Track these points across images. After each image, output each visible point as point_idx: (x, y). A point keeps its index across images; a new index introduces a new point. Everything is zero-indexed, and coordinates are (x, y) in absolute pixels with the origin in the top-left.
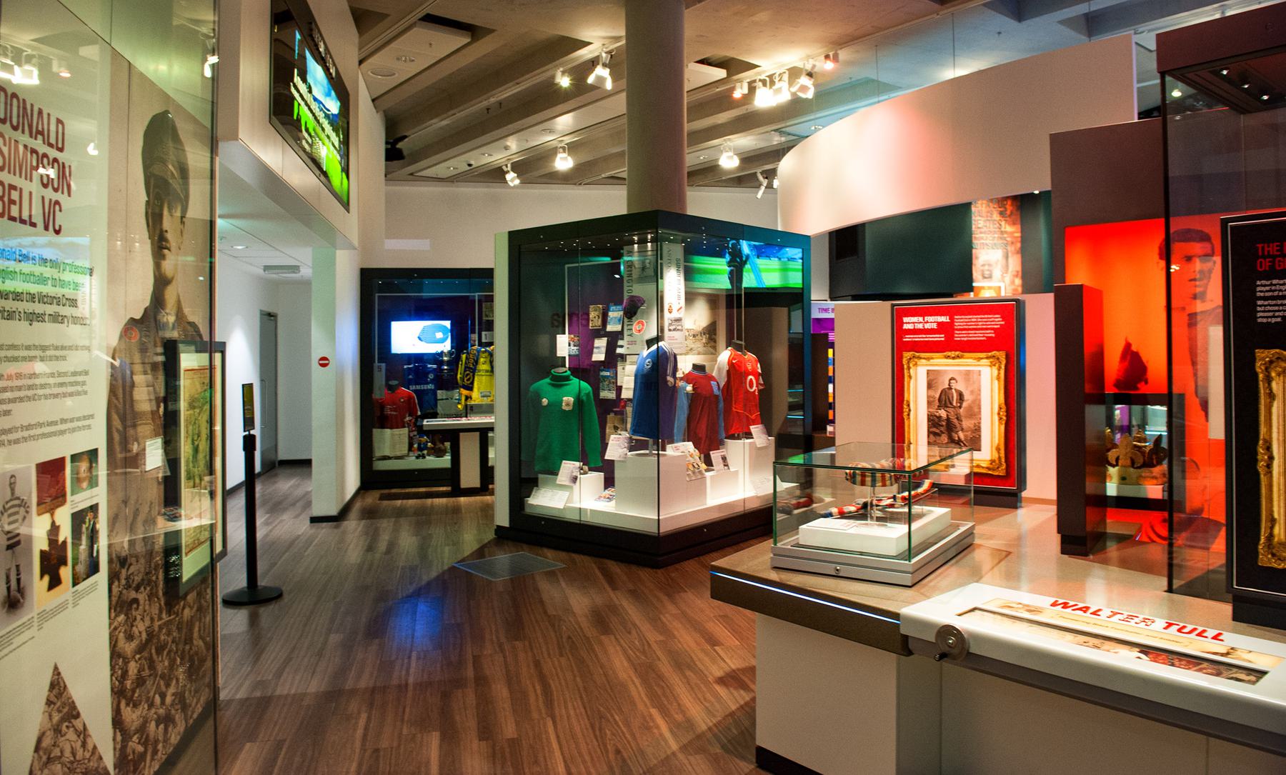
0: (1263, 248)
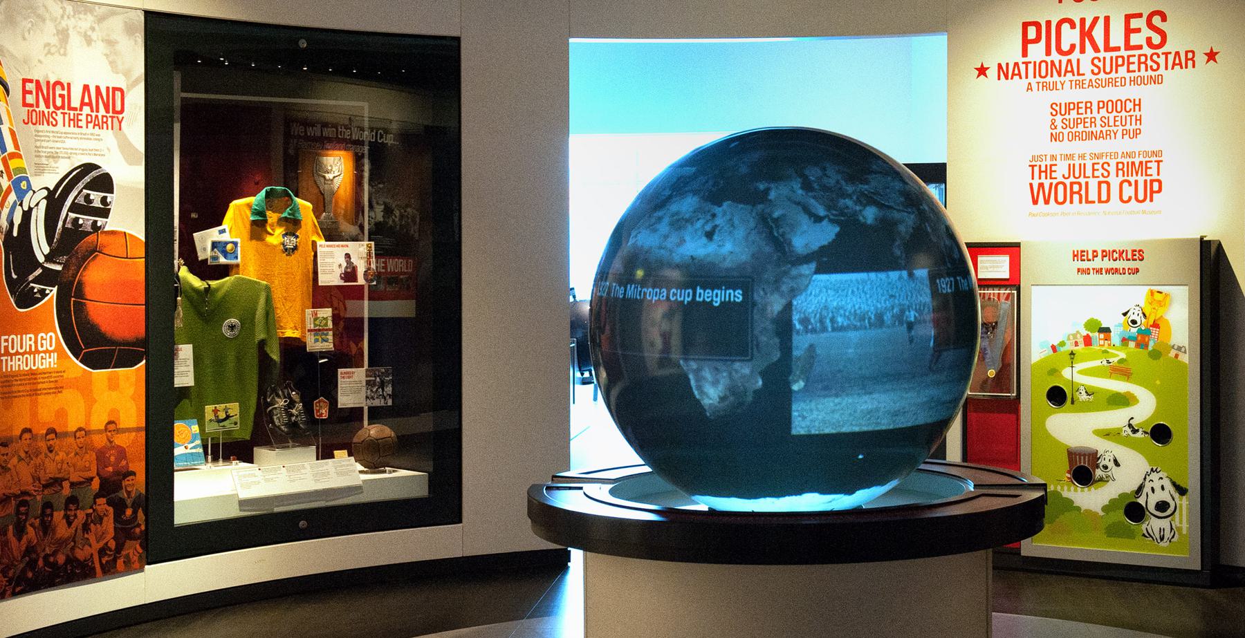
0: (7, 360)
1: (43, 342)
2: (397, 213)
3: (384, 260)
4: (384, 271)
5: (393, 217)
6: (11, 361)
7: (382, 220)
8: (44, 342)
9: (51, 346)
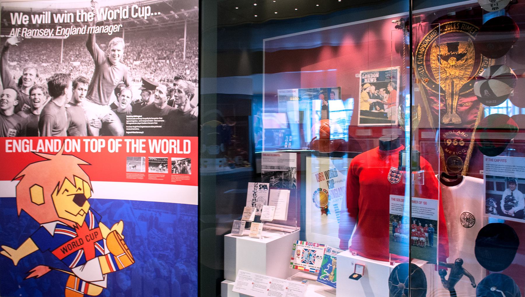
0: (130, 143)
1: (27, 146)
2: (163, 88)
3: (144, 140)
4: (144, 152)
5: (157, 93)
6: (135, 143)
7: (140, 98)
8: (27, 146)
9: (112, 142)
